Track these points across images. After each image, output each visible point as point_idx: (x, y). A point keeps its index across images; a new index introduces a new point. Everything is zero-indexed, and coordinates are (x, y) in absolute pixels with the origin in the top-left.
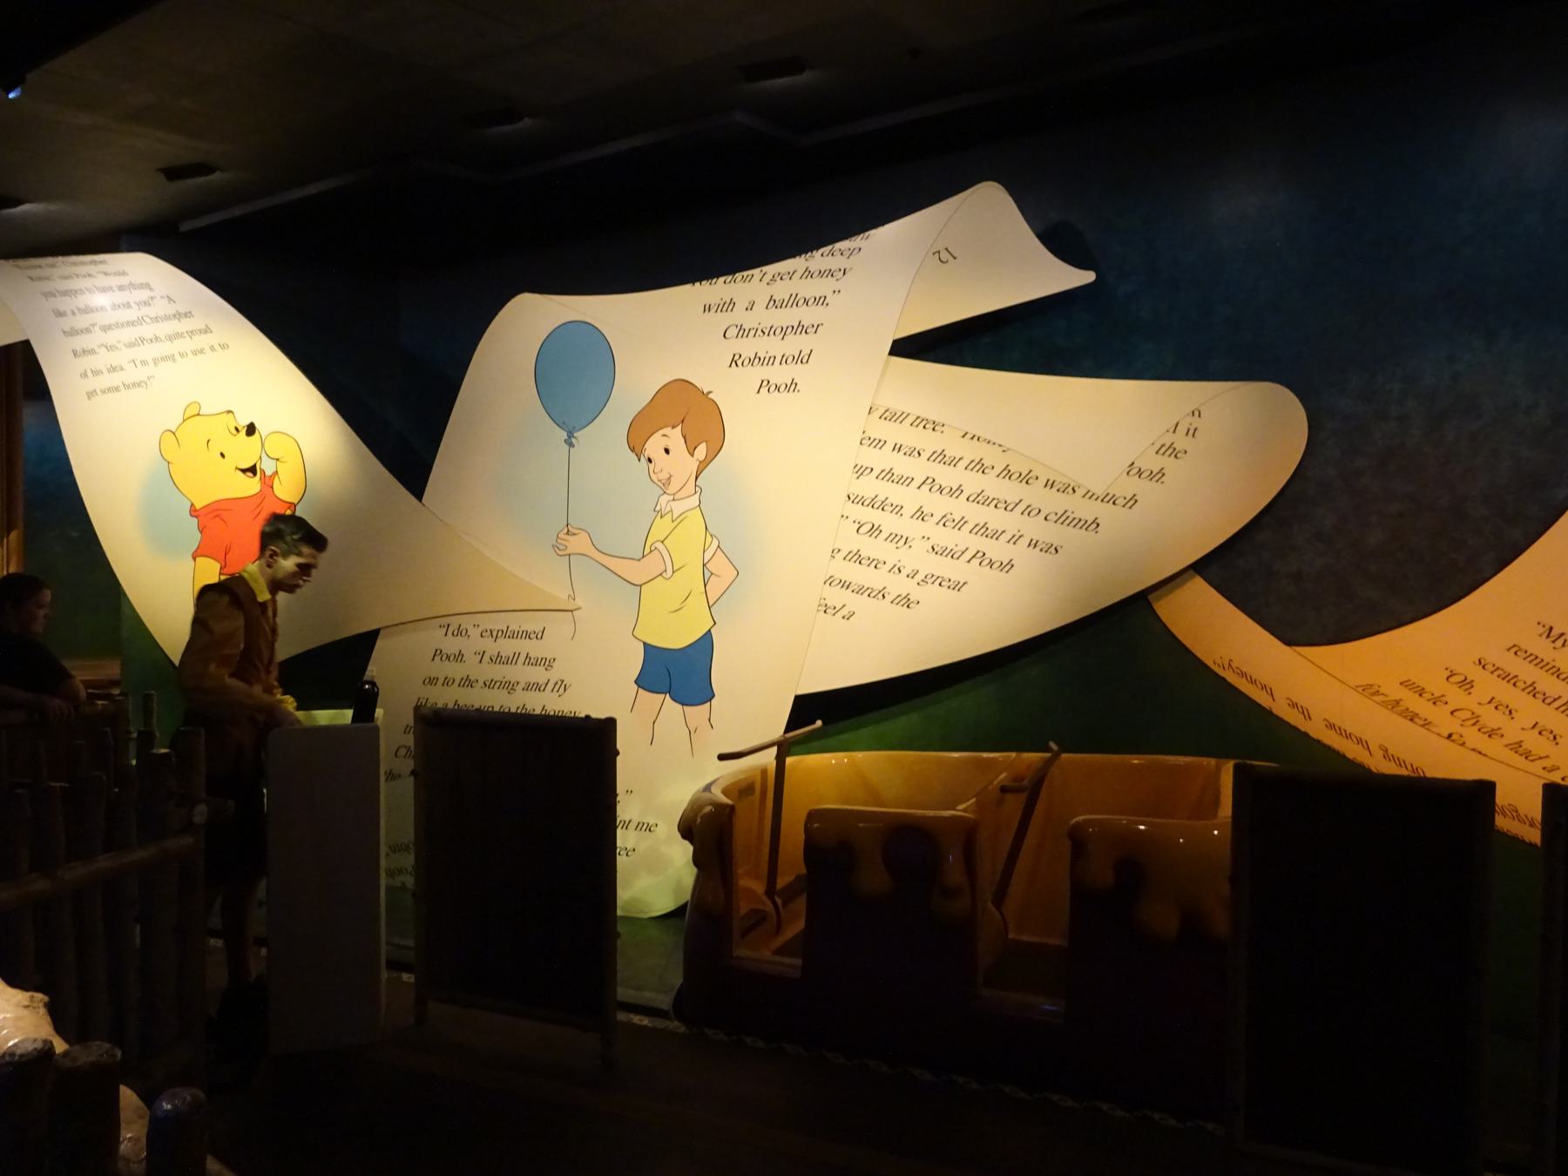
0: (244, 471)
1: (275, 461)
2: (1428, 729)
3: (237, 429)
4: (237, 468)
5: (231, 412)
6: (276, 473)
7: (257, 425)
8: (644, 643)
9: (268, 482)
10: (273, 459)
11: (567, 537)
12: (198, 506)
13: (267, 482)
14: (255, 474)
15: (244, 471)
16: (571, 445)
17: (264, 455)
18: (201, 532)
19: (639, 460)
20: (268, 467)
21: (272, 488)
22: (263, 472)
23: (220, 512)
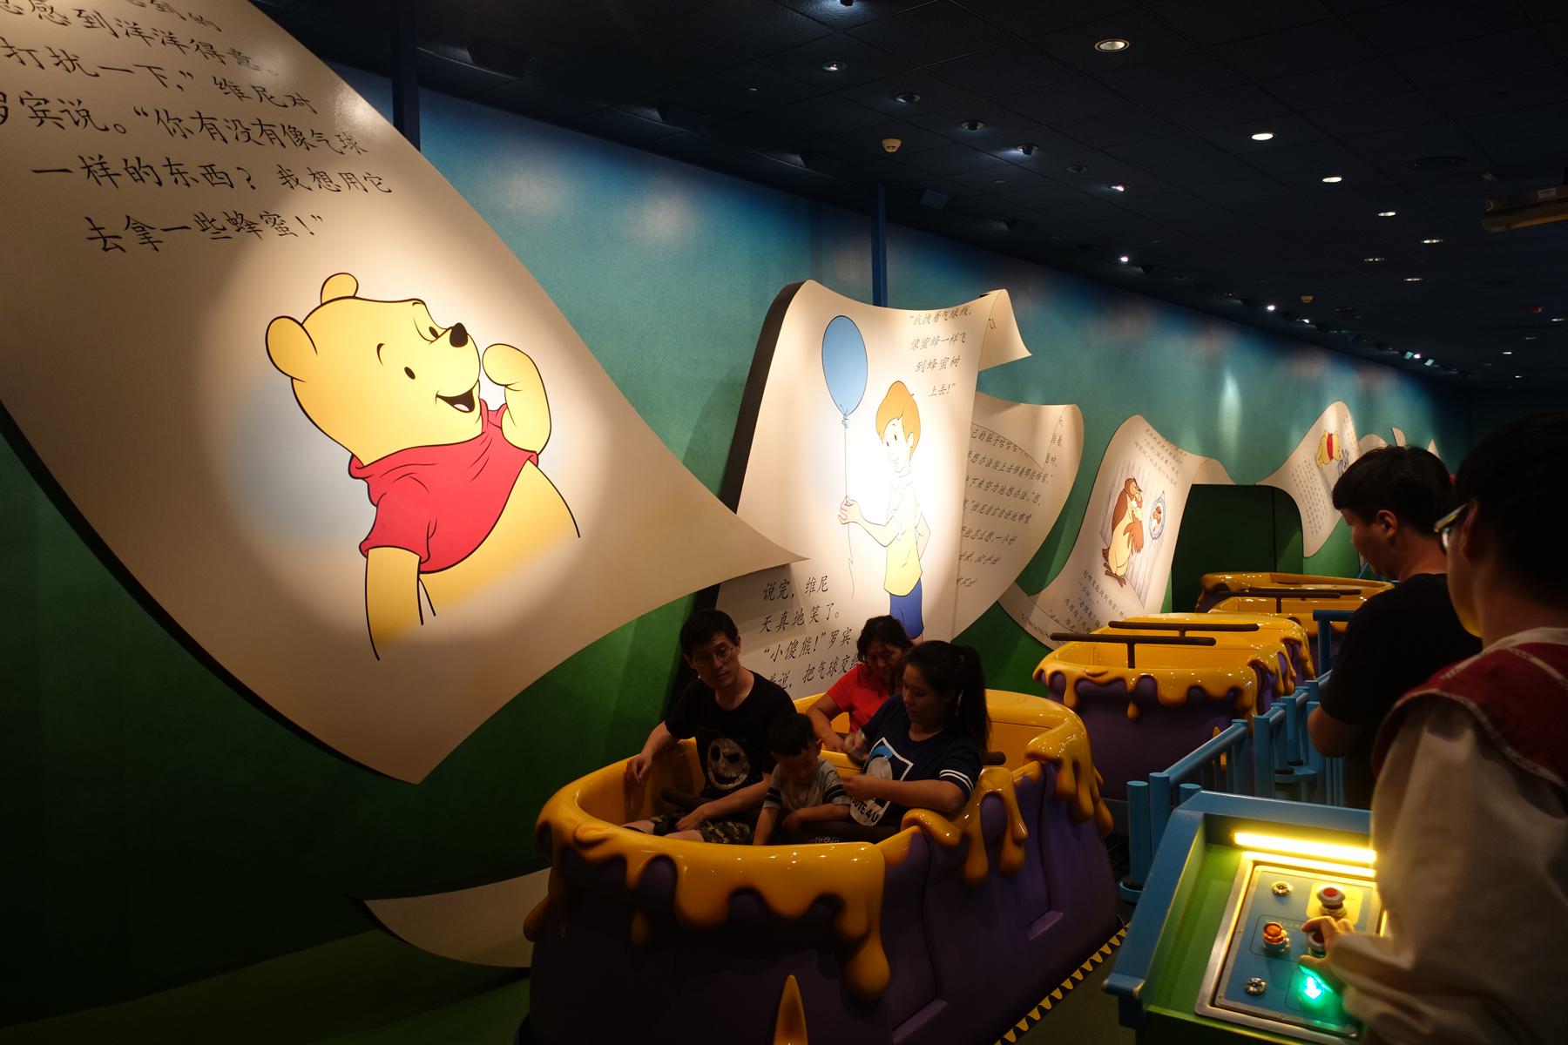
0: (452, 401)
3: (433, 331)
4: (437, 396)
9: (493, 419)
14: (471, 408)
15: (452, 401)
17: (483, 379)
18: (377, 506)
20: (493, 397)
21: (501, 428)
22: (483, 403)
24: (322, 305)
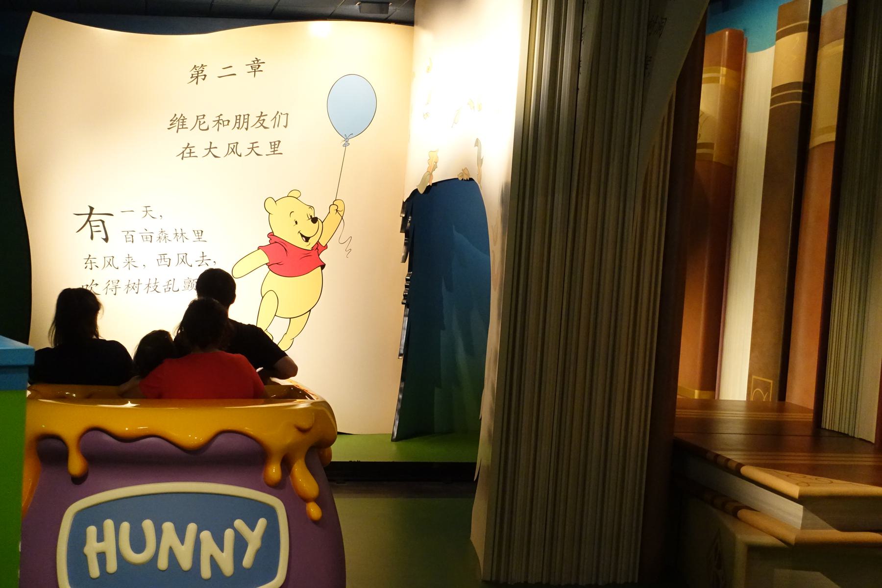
24: (288, 196)
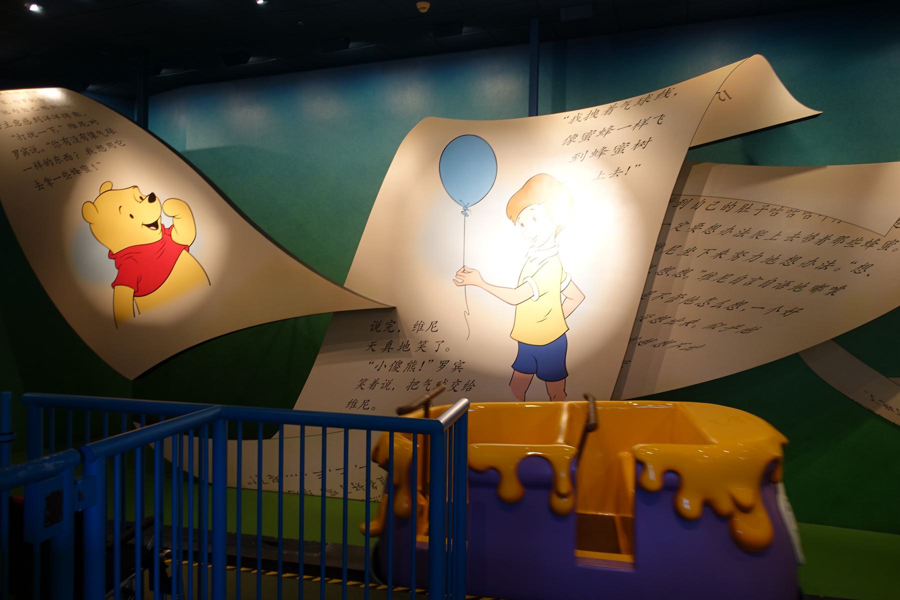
0: (149, 226)
1: (172, 218)
2: (833, 218)
5: (137, 187)
6: (173, 226)
7: (156, 195)
8: (518, 342)
9: (167, 232)
10: (94, 205)
11: (463, 274)
12: (115, 252)
13: (166, 232)
14: (157, 228)
15: (149, 226)
16: (466, 215)
19: (515, 225)
21: (171, 235)
22: (163, 226)
23: (131, 255)
